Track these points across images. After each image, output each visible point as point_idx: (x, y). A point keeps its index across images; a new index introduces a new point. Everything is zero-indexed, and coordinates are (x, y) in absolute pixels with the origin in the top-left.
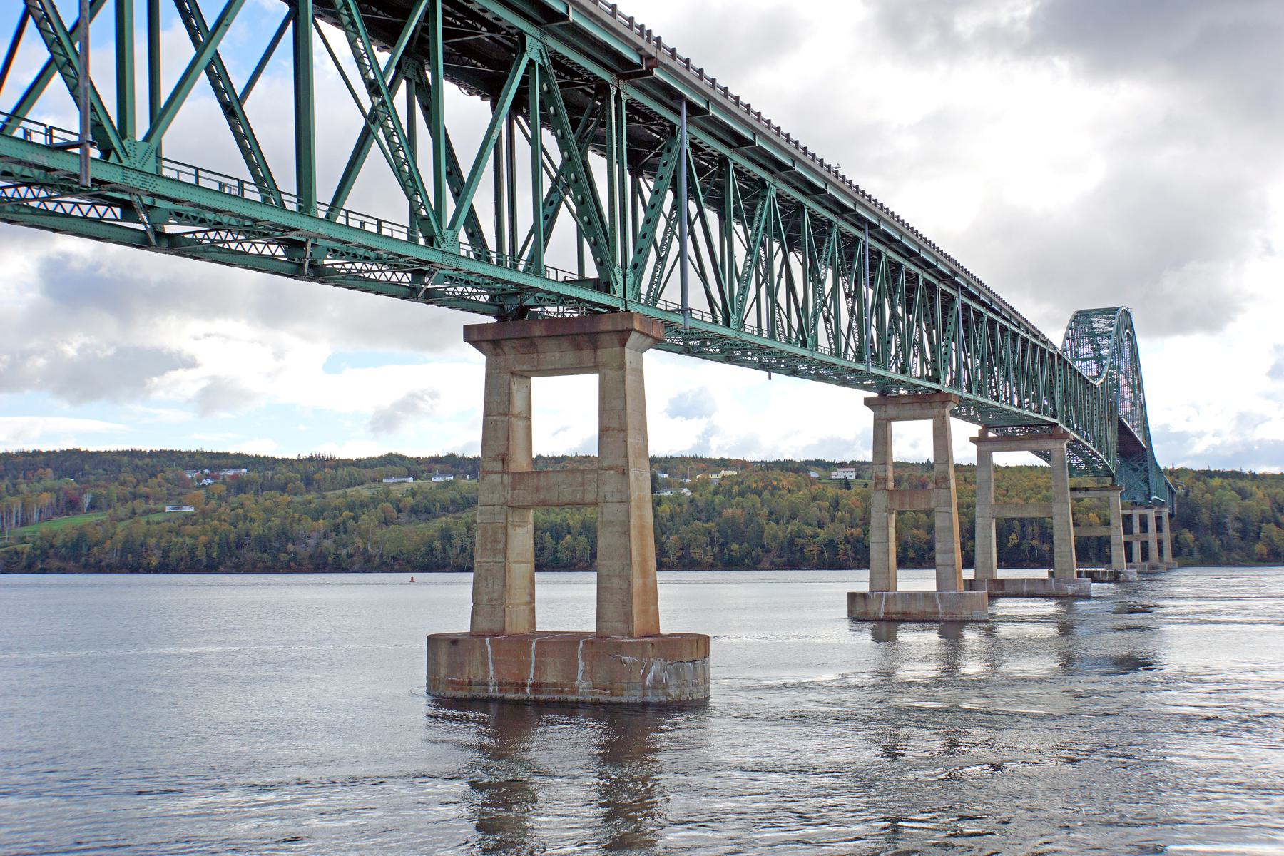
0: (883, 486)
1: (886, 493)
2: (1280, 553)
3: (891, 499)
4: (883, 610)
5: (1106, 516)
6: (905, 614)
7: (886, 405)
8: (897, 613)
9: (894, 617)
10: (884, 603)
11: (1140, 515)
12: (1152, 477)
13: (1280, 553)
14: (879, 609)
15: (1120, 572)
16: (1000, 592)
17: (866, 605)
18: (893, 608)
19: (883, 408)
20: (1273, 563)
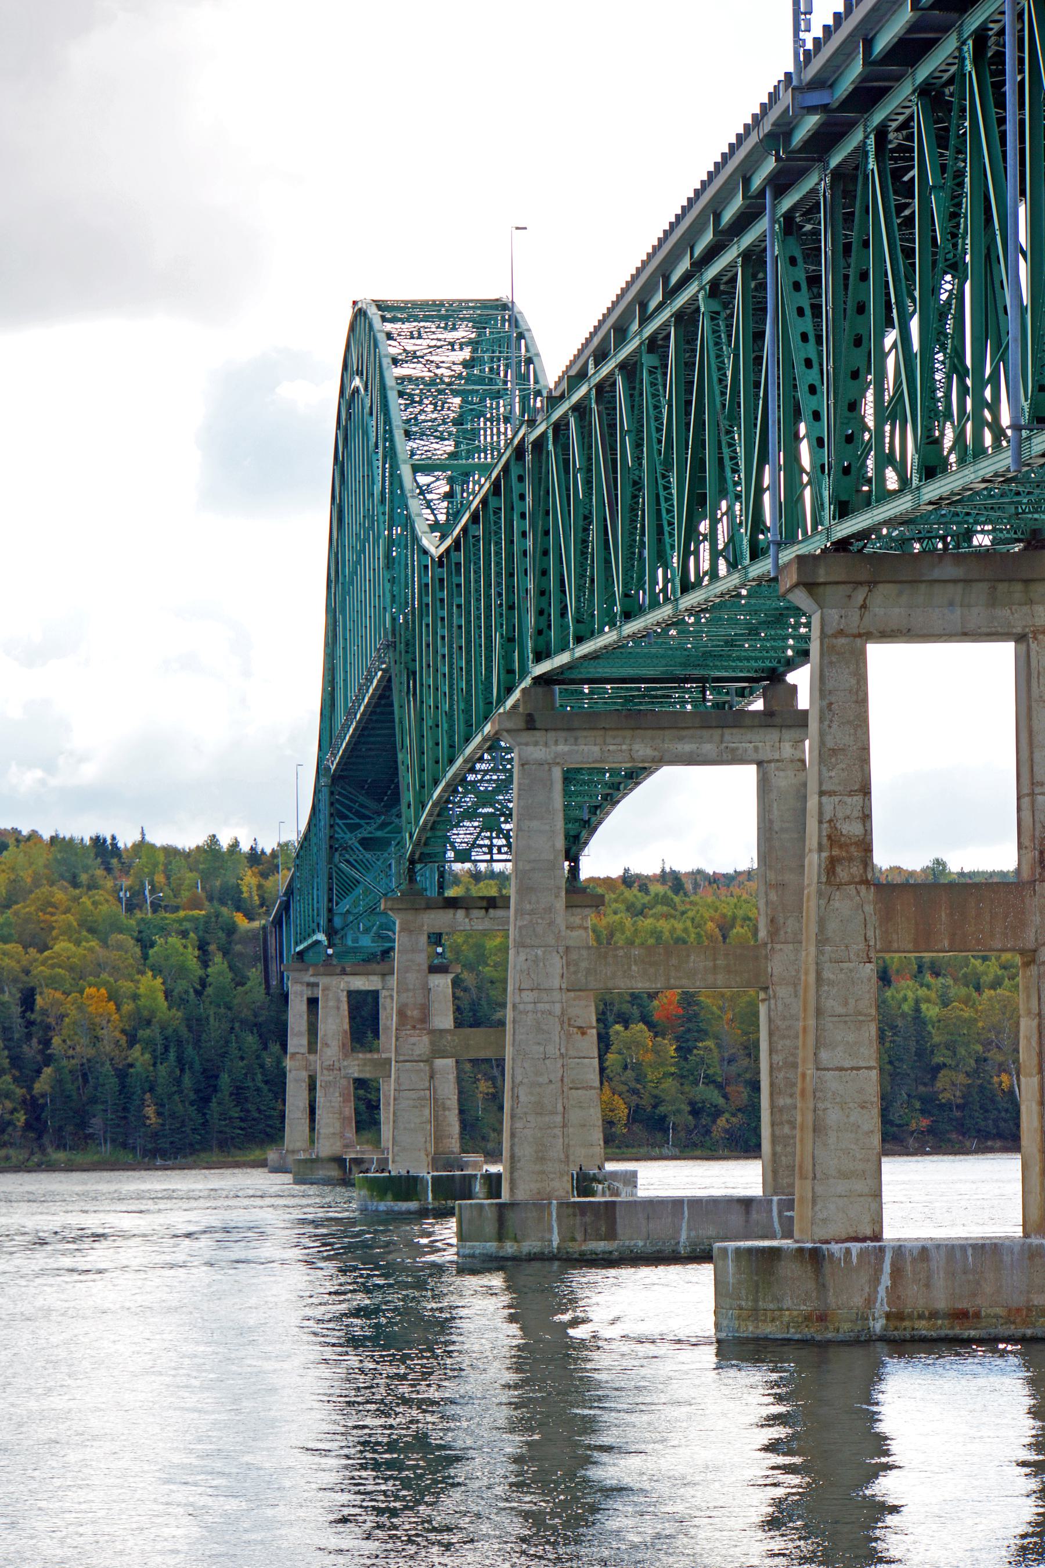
0: (856, 870)
1: (868, 895)
2: (663, 1118)
3: (887, 916)
4: (882, 1306)
5: (135, 997)
6: (961, 1316)
7: (872, 584)
8: (934, 1315)
9: (923, 1328)
10: (886, 1280)
11: (350, 993)
12: (869, 869)
13: (663, 1118)
14: (870, 1302)
15: (595, 1179)
16: (601, 1246)
17: (822, 1287)
18: (915, 1298)
19: (860, 596)
20: (643, 1150)
